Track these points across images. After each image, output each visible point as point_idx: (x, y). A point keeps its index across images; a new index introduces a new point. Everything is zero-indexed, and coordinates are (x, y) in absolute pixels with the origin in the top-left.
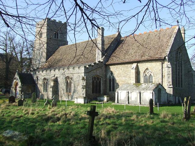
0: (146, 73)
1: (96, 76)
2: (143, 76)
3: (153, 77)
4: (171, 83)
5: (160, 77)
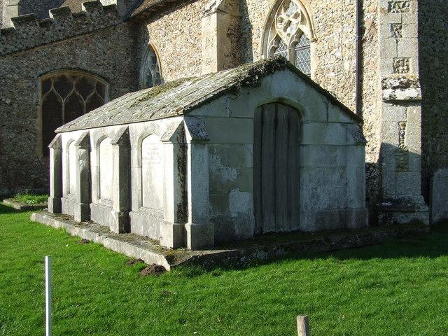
0: (279, 28)
1: (67, 74)
2: (264, 45)
3: (313, 46)
4: (413, 73)
5: (346, 42)
